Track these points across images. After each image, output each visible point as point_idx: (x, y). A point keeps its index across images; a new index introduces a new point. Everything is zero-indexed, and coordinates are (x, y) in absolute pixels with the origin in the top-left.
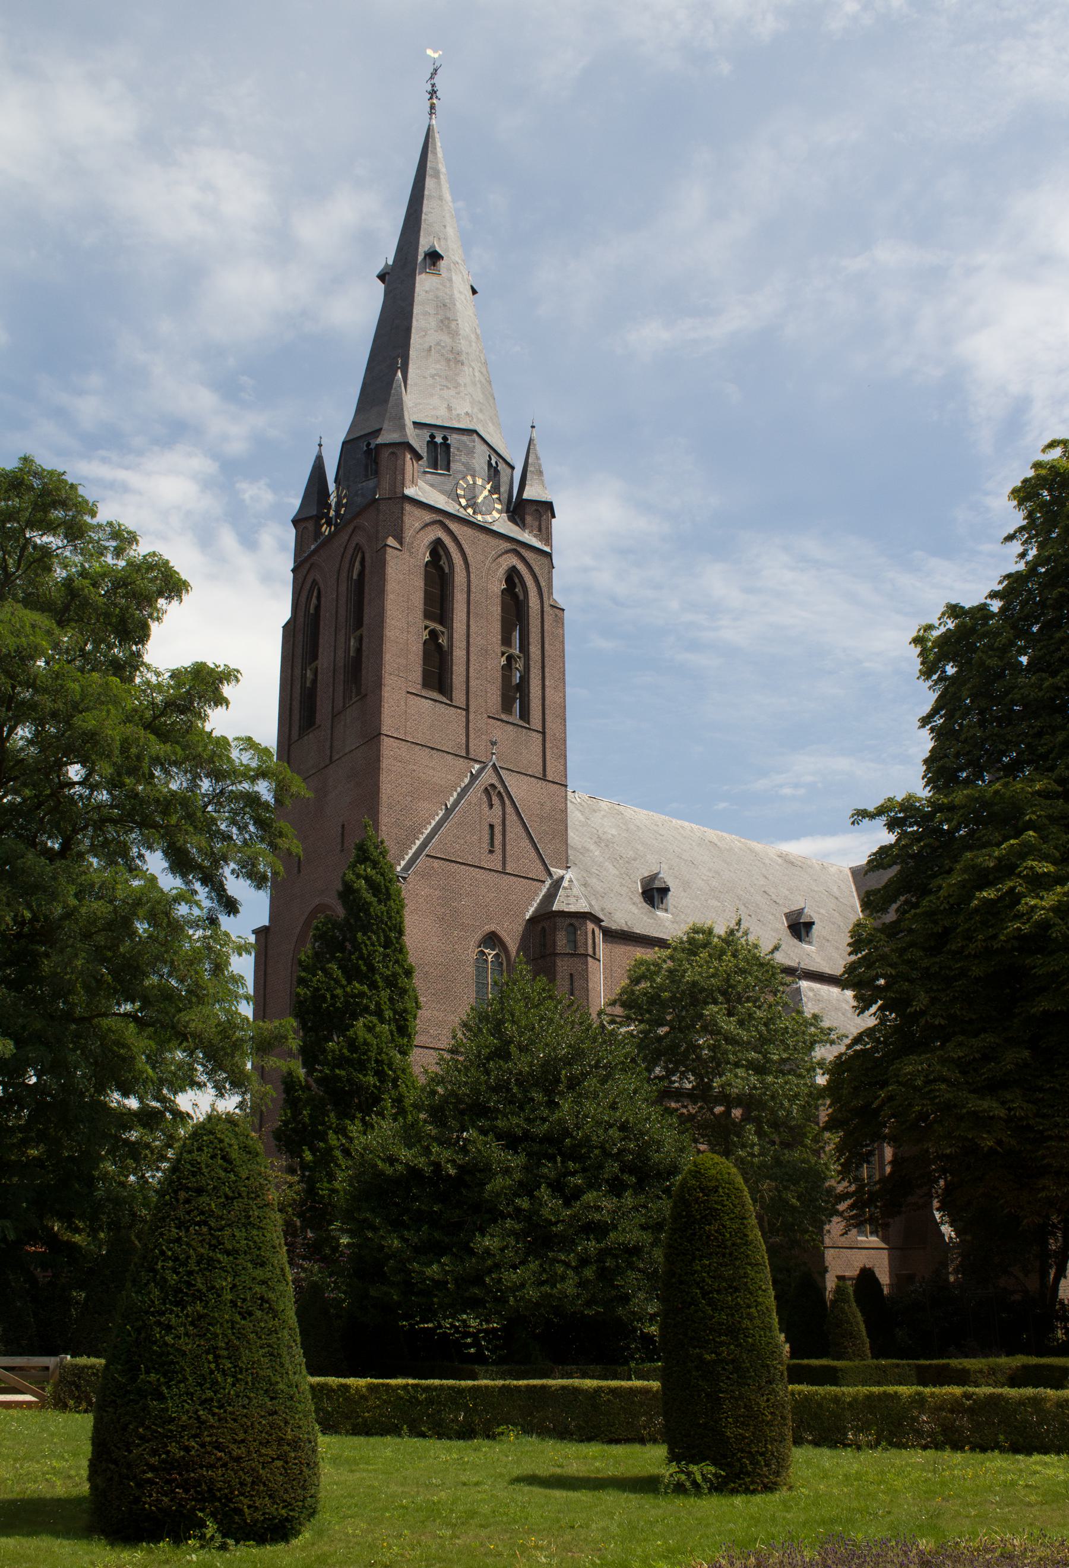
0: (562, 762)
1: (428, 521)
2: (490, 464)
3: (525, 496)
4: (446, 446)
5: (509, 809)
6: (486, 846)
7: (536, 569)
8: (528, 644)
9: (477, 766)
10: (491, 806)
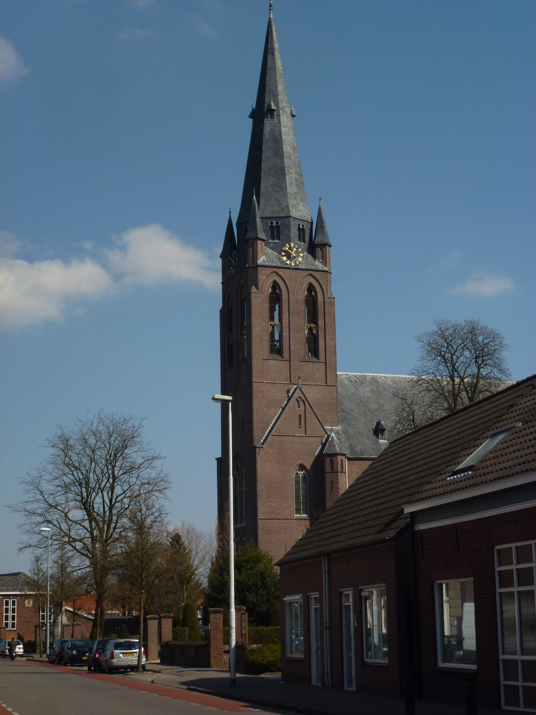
2: (299, 228)
4: (278, 227)
5: (308, 406)
6: (297, 425)
7: (321, 281)
9: (295, 387)
10: (299, 407)
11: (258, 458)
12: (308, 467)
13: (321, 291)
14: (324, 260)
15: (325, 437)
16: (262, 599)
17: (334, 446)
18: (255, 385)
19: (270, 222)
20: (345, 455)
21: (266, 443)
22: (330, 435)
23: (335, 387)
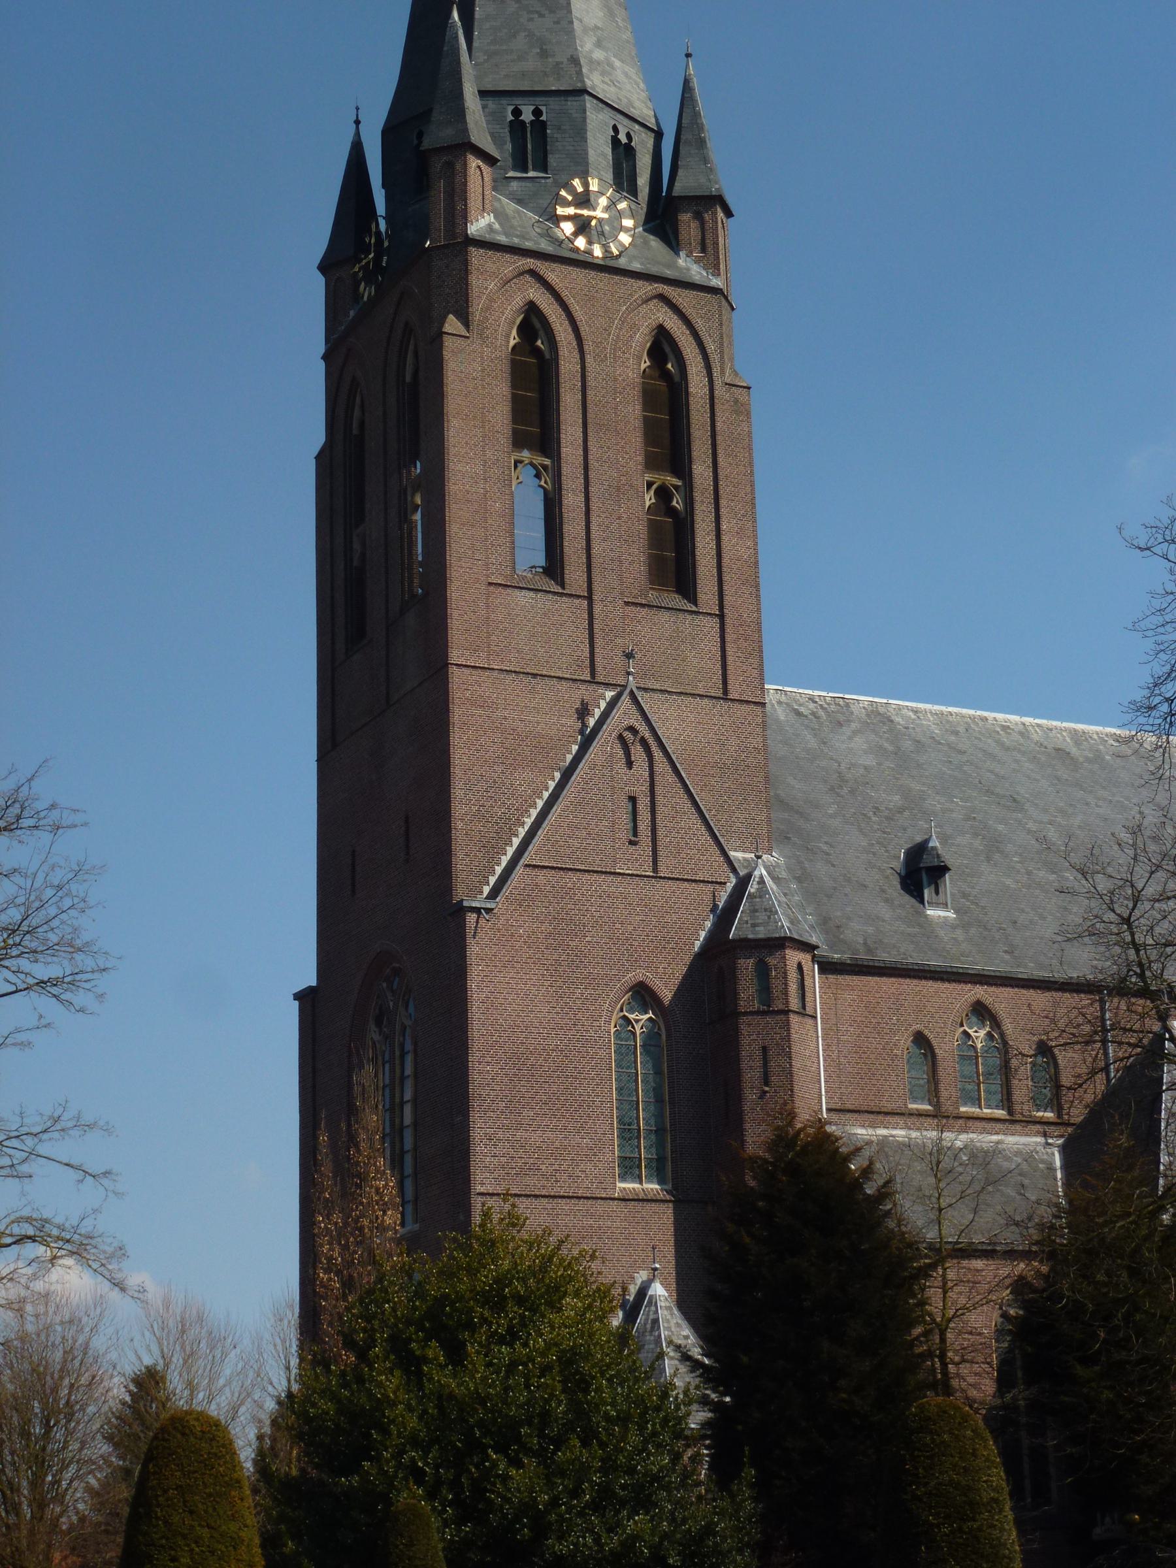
0: (755, 662)
1: (510, 275)
2: (615, 141)
3: (675, 193)
4: (540, 126)
6: (624, 834)
7: (699, 324)
8: (690, 462)
9: (609, 694)
10: (630, 764)
11: (474, 949)
12: (666, 994)
13: (699, 358)
14: (708, 251)
15: (730, 886)
16: (576, 1493)
17: (771, 911)
18: (457, 678)
19: (510, 108)
20: (808, 947)
21: (506, 891)
22: (749, 876)
23: (759, 709)
